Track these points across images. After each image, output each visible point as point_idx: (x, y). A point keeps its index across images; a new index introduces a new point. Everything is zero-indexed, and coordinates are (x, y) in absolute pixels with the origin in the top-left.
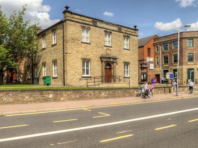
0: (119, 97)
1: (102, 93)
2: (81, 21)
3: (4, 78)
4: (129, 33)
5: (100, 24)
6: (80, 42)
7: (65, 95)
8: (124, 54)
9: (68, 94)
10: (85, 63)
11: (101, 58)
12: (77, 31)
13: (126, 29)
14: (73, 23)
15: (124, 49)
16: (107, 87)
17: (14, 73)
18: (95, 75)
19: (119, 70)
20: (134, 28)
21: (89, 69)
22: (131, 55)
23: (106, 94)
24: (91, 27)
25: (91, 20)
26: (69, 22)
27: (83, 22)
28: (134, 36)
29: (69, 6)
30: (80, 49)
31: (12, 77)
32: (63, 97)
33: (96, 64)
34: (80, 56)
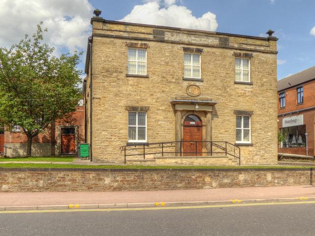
0: (155, 188)
1: (106, 179)
2: (126, 35)
3: (56, 147)
4: (249, 47)
5: (172, 36)
6: (123, 76)
7: (11, 180)
8: (237, 95)
9: (19, 179)
10: (241, 119)
11: (174, 104)
12: (117, 54)
13: (243, 39)
14: (108, 40)
15: (236, 83)
16: (175, 165)
17: (71, 138)
18: (159, 140)
19: (221, 128)
20: (267, 36)
21: (250, 131)
22: (254, 95)
23: (117, 181)
24: (151, 44)
25: (150, 30)
26: (100, 38)
27: (132, 35)
28: (263, 52)
29: (273, 30)
30: (123, 88)
31: (68, 146)
32: (8, 183)
33: (161, 118)
34: (123, 103)
